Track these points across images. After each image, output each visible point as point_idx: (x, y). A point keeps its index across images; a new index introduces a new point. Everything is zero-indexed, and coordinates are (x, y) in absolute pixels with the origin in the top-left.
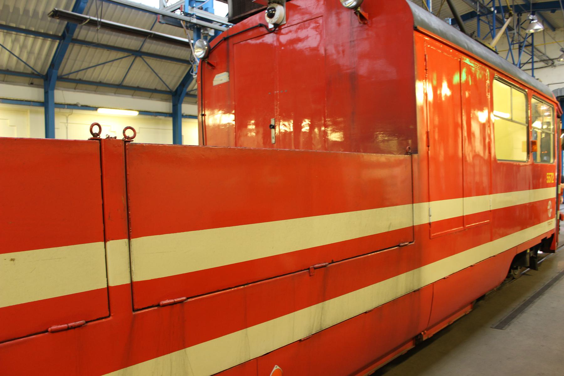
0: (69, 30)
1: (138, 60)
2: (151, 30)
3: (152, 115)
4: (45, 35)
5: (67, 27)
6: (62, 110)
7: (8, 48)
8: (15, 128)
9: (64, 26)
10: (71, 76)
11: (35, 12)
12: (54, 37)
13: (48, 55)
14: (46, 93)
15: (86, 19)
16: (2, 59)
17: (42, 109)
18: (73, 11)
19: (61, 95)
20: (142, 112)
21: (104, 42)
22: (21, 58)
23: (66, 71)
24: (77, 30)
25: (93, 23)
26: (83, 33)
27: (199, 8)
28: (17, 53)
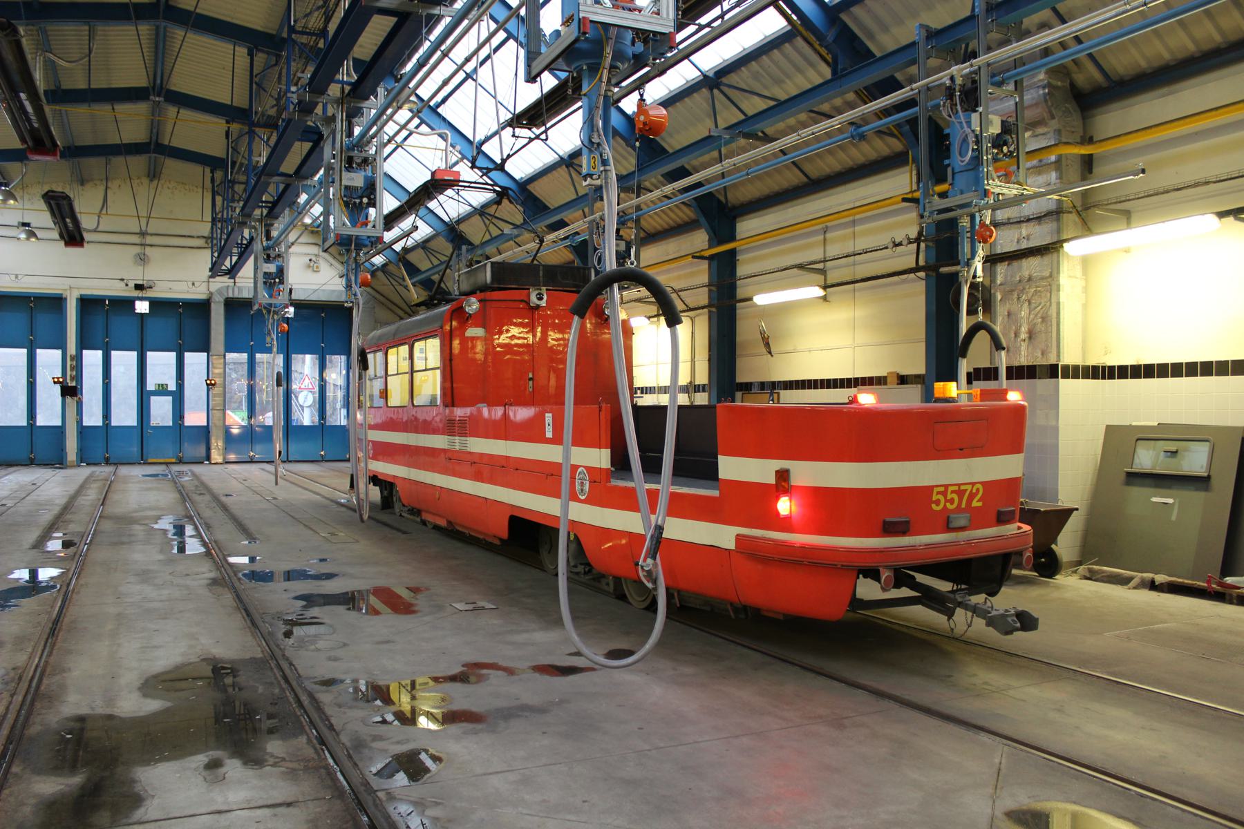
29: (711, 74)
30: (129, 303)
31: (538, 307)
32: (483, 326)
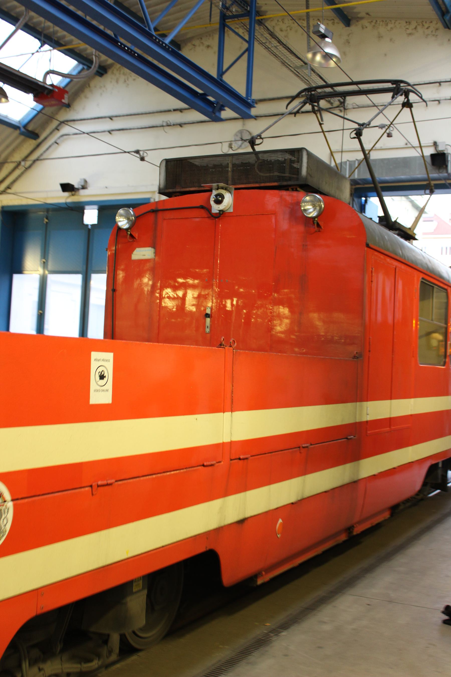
30: (78, 209)
31: (222, 213)
32: (153, 246)
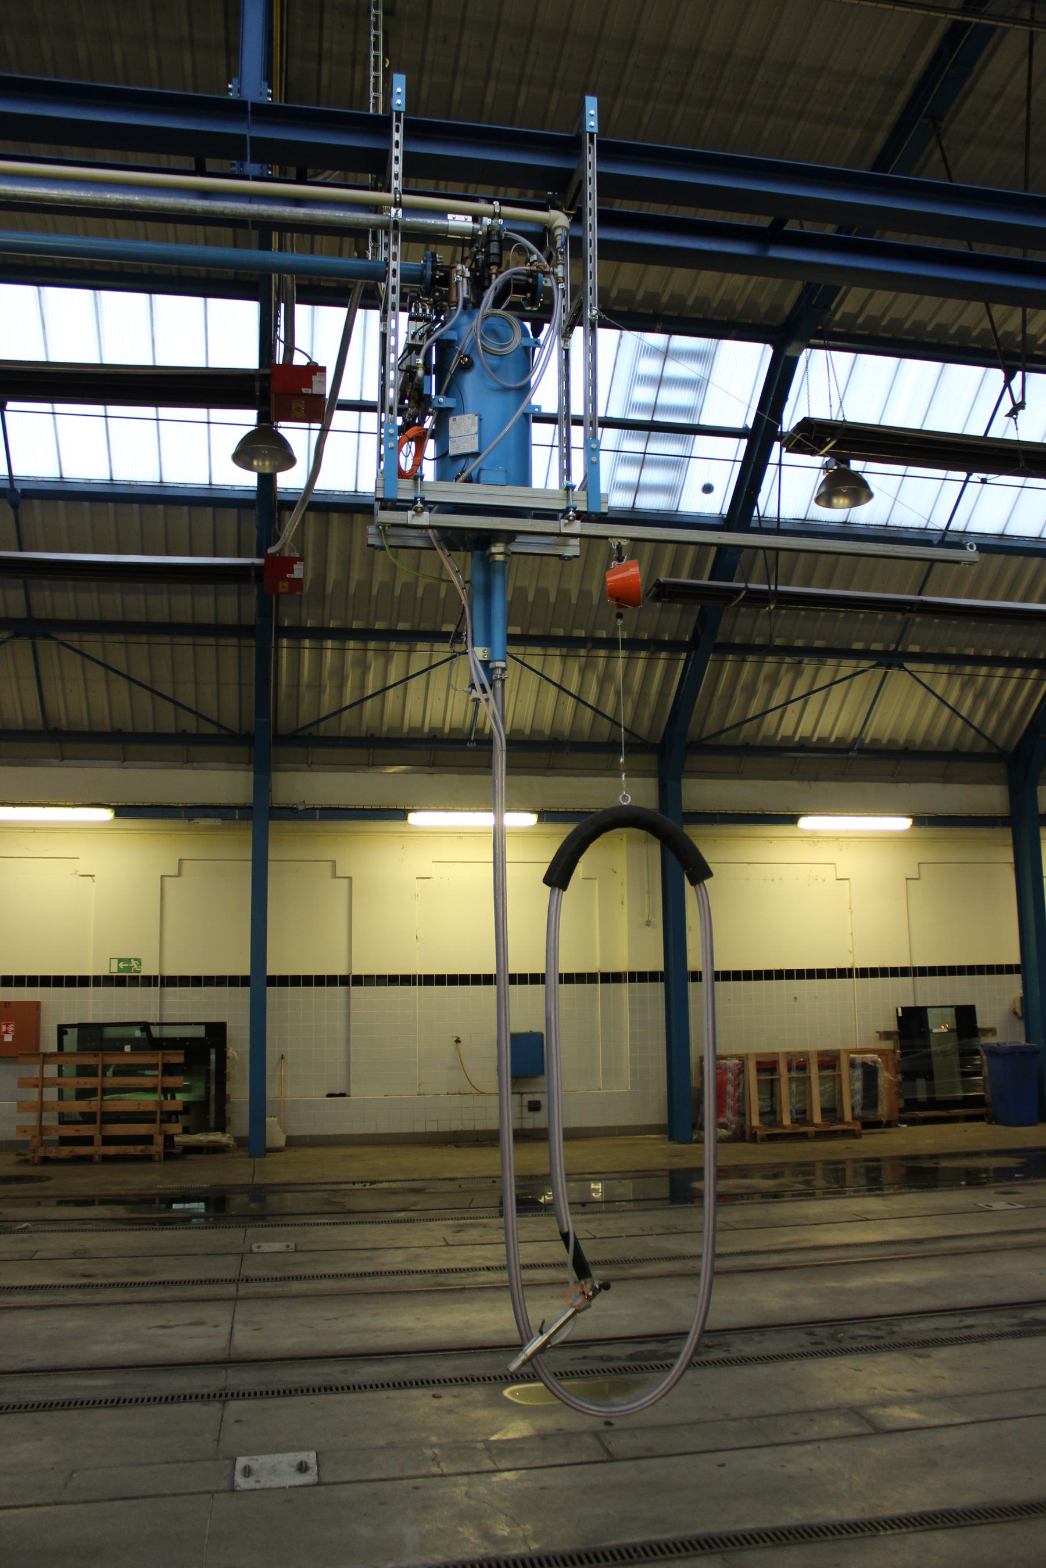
0: (705, 625)
1: (895, 673)
2: (919, 594)
3: (178, 817)
4: (654, 645)
5: (702, 617)
6: (288, 825)
7: (573, 690)
8: (596, 882)
9: (694, 618)
10: (723, 739)
11: (584, 594)
12: (674, 646)
13: (663, 693)
14: (662, 788)
15: (738, 591)
16: (19, 704)
17: (1006, 834)
18: (711, 578)
19: (701, 792)
20: (122, 811)
21: (160, 616)
22: (600, 709)
23: (711, 726)
24: (725, 622)
25: (757, 598)
26: (742, 624)
27: (466, 481)
28: (591, 700)
29: (19, 487)
